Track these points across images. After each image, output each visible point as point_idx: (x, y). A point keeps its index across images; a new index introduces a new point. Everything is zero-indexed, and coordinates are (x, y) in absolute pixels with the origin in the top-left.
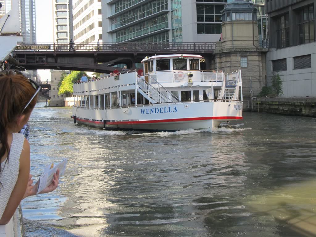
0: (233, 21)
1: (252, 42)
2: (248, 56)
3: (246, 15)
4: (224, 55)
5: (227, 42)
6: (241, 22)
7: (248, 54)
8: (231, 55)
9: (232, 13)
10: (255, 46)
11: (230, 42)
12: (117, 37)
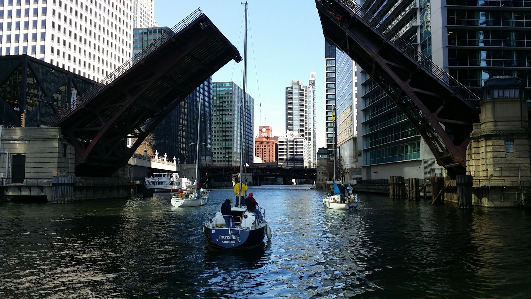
0: (495, 99)
1: (520, 123)
2: (516, 139)
3: (512, 92)
4: (484, 139)
5: (488, 123)
6: (506, 100)
7: (514, 137)
8: (463, 187)
9: (494, 89)
10: (523, 127)
11: (491, 123)
12: (370, 127)
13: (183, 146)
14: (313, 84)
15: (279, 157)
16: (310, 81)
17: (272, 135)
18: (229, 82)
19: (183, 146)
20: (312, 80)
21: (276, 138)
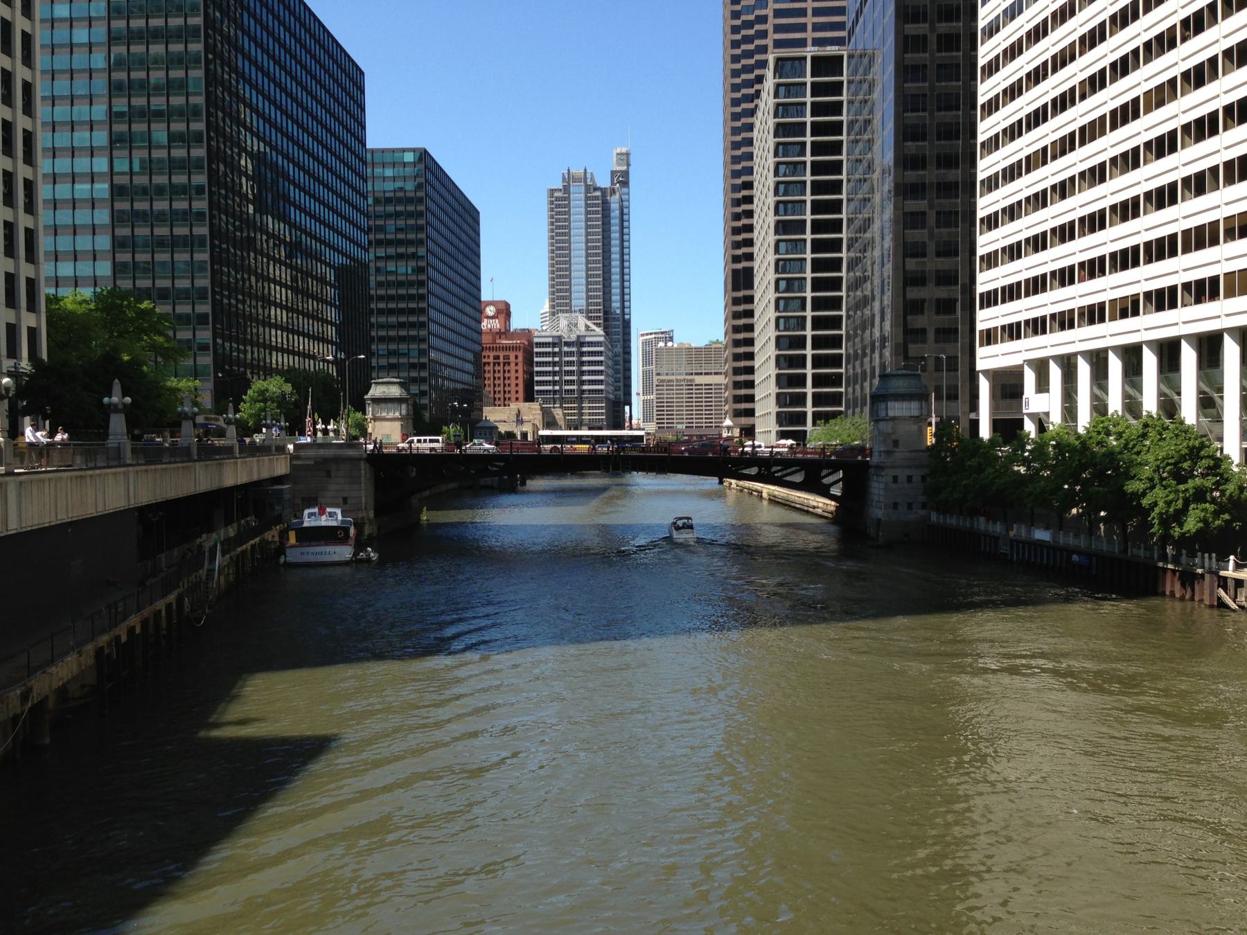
13: (280, 360)
14: (625, 183)
15: (536, 388)
16: (613, 173)
17: (517, 323)
18: (414, 150)
19: (280, 360)
20: (618, 171)
21: (527, 333)
